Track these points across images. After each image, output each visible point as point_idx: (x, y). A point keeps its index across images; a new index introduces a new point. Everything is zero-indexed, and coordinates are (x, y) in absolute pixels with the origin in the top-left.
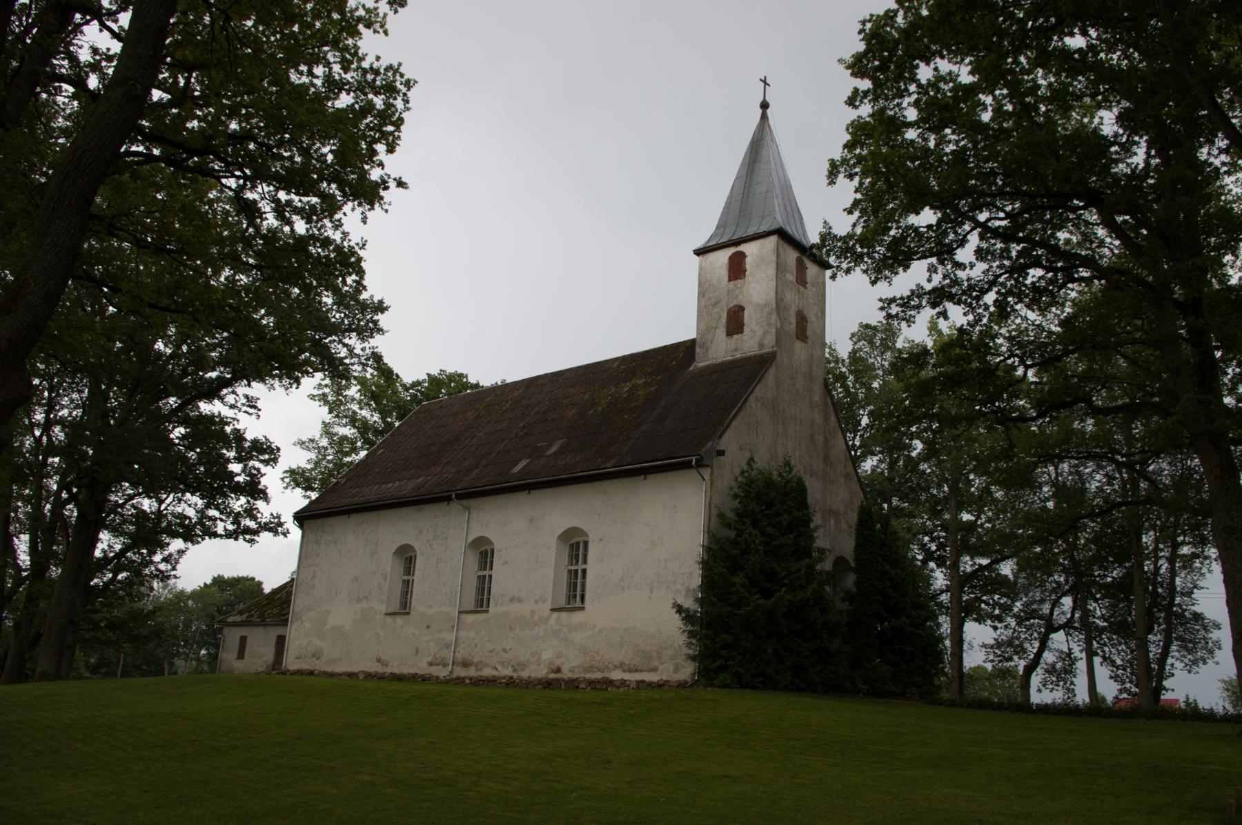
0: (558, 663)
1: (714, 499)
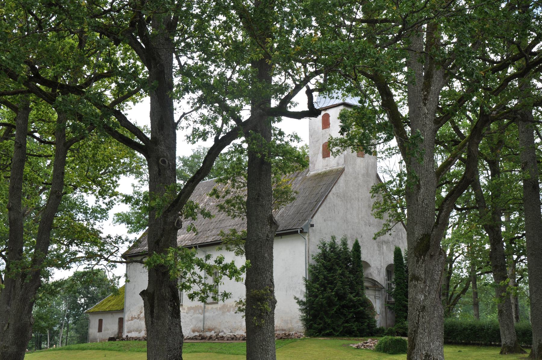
1: (310, 248)
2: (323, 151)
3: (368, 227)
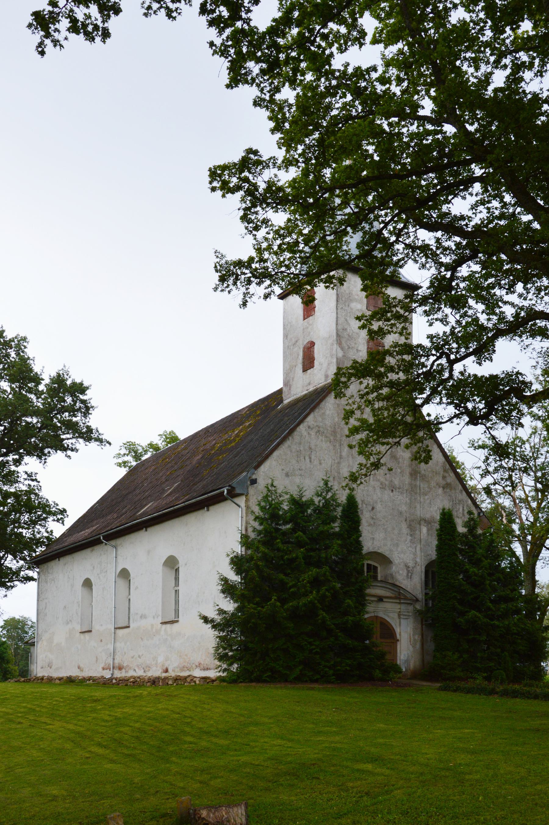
0: (166, 665)
2: (303, 359)
3: (388, 492)
